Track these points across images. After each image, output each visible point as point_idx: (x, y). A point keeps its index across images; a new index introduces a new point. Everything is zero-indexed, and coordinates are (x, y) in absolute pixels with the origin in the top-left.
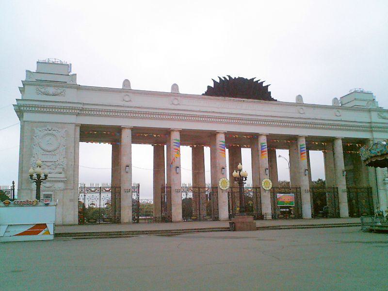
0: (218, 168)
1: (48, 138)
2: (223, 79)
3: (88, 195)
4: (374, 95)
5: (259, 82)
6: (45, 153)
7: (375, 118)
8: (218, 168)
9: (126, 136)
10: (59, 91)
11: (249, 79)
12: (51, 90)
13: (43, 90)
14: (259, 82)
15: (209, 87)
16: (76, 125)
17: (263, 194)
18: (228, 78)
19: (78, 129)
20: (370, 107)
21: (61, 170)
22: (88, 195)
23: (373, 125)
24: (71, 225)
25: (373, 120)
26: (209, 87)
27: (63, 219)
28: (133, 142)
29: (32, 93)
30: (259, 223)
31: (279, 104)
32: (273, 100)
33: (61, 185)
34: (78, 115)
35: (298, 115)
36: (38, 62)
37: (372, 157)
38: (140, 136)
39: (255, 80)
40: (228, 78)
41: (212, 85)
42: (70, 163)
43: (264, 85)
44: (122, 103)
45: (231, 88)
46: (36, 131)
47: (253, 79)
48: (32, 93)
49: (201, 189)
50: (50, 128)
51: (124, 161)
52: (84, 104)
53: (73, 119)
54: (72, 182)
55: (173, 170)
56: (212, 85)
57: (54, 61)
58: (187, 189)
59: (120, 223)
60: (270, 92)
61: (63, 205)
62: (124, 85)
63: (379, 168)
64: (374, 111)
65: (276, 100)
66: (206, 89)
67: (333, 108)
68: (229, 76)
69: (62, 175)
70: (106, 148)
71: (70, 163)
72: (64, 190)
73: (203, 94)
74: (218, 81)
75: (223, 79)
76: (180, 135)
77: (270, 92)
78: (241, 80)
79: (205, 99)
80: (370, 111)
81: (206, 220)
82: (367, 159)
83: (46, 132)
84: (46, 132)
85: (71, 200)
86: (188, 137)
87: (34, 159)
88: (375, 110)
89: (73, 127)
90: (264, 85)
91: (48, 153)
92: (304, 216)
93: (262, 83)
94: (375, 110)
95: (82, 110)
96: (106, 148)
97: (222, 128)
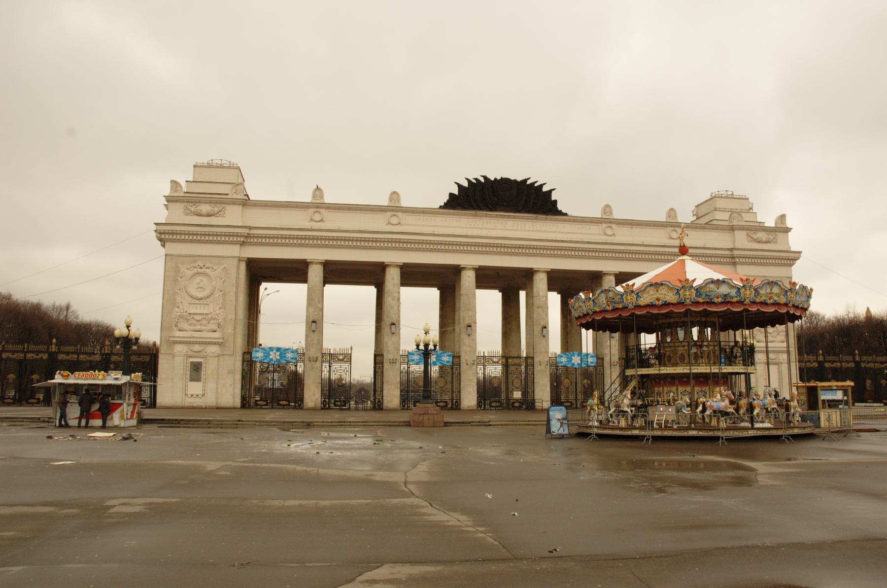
0: (462, 325)
1: (198, 279)
2: (474, 181)
3: (335, 366)
4: (751, 200)
5: (536, 185)
6: (194, 301)
7: (741, 240)
8: (537, 329)
9: (393, 276)
10: (216, 210)
11: (519, 180)
12: (205, 208)
13: (193, 209)
14: (536, 185)
15: (451, 195)
16: (240, 260)
17: (537, 368)
18: (482, 180)
19: (243, 266)
20: (735, 223)
21: (215, 327)
22: (335, 366)
23: (736, 253)
24: (230, 408)
25: (738, 245)
26: (451, 195)
27: (217, 399)
28: (403, 284)
29: (180, 215)
30: (450, 417)
31: (569, 221)
32: (560, 213)
33: (214, 349)
34: (243, 244)
35: (603, 239)
36: (195, 166)
37: (595, 313)
38: (414, 275)
39: (529, 182)
40: (482, 180)
41: (456, 191)
42: (230, 317)
43: (545, 189)
44: (309, 225)
45: (483, 196)
46: (183, 268)
47: (525, 180)
48: (180, 215)
49: (510, 360)
50: (201, 265)
51: (463, 315)
52: (250, 228)
53: (234, 251)
54: (232, 345)
55: (386, 330)
56: (456, 191)
57: (219, 162)
58: (485, 360)
59: (460, 409)
60: (556, 201)
61: (218, 379)
62: (391, 200)
63: (770, 329)
64: (740, 229)
65: (566, 214)
66: (446, 198)
67: (601, 223)
68: (485, 177)
69: (216, 335)
70: (432, 295)
71: (230, 317)
72: (218, 356)
73: (441, 207)
74: (466, 184)
75: (474, 181)
76: (401, 273)
77: (556, 201)
78: (505, 182)
79: (443, 214)
80: (732, 229)
81: (261, 407)
82: (585, 316)
83: (196, 270)
84: (196, 270)
85: (230, 372)
86: (487, 278)
87: (177, 310)
88: (742, 228)
89: (235, 262)
90: (545, 189)
91: (197, 302)
92: (538, 405)
93: (541, 186)
94: (742, 228)
95: (248, 236)
96: (432, 295)
97: (543, 264)
